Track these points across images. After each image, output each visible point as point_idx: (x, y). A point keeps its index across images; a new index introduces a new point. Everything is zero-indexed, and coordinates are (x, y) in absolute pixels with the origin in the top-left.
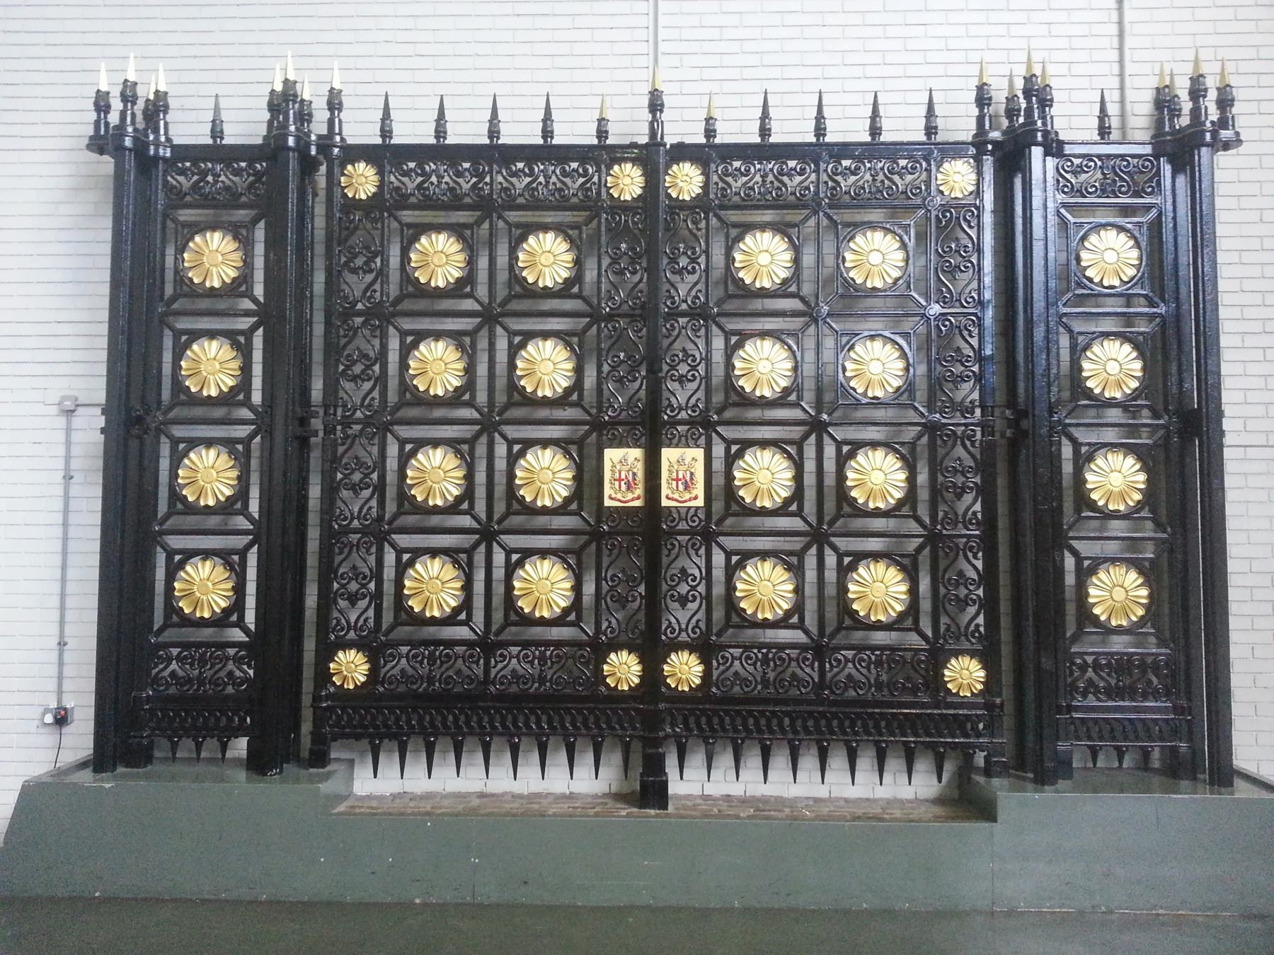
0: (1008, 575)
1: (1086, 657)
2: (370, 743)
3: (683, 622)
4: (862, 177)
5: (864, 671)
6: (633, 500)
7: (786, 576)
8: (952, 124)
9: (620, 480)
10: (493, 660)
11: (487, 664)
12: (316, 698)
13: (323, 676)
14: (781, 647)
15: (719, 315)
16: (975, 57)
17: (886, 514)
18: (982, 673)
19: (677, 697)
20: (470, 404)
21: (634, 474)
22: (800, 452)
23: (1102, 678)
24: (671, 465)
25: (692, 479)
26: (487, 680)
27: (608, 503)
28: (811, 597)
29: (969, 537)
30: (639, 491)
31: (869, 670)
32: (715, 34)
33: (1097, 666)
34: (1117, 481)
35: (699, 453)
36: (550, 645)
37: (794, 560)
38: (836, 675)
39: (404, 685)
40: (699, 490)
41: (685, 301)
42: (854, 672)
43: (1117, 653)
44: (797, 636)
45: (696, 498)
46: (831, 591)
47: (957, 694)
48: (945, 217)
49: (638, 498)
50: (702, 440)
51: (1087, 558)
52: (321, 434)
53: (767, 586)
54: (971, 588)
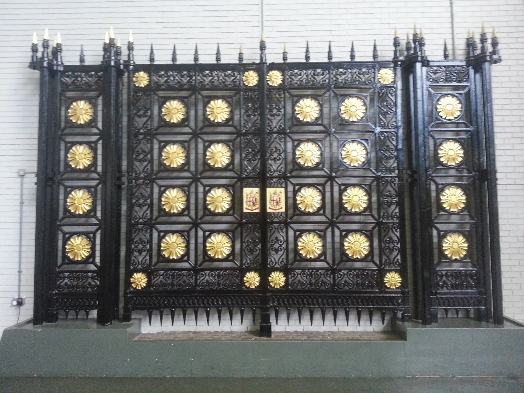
5: (352, 279)
6: (255, 209)
7: (319, 240)
8: (384, 54)
11: (334, 277)
12: (125, 293)
13: (128, 284)
14: (317, 269)
15: (290, 133)
16: (393, 26)
18: (400, 279)
19: (136, 291)
20: (188, 171)
22: (324, 189)
25: (279, 200)
26: (196, 285)
27: (245, 211)
30: (258, 206)
31: (353, 279)
33: (447, 276)
35: (282, 190)
37: (322, 233)
40: (283, 205)
42: (347, 279)
44: (324, 265)
45: (281, 208)
46: (337, 246)
49: (257, 209)
50: (284, 185)
51: (442, 231)
52: (126, 184)
54: (395, 244)
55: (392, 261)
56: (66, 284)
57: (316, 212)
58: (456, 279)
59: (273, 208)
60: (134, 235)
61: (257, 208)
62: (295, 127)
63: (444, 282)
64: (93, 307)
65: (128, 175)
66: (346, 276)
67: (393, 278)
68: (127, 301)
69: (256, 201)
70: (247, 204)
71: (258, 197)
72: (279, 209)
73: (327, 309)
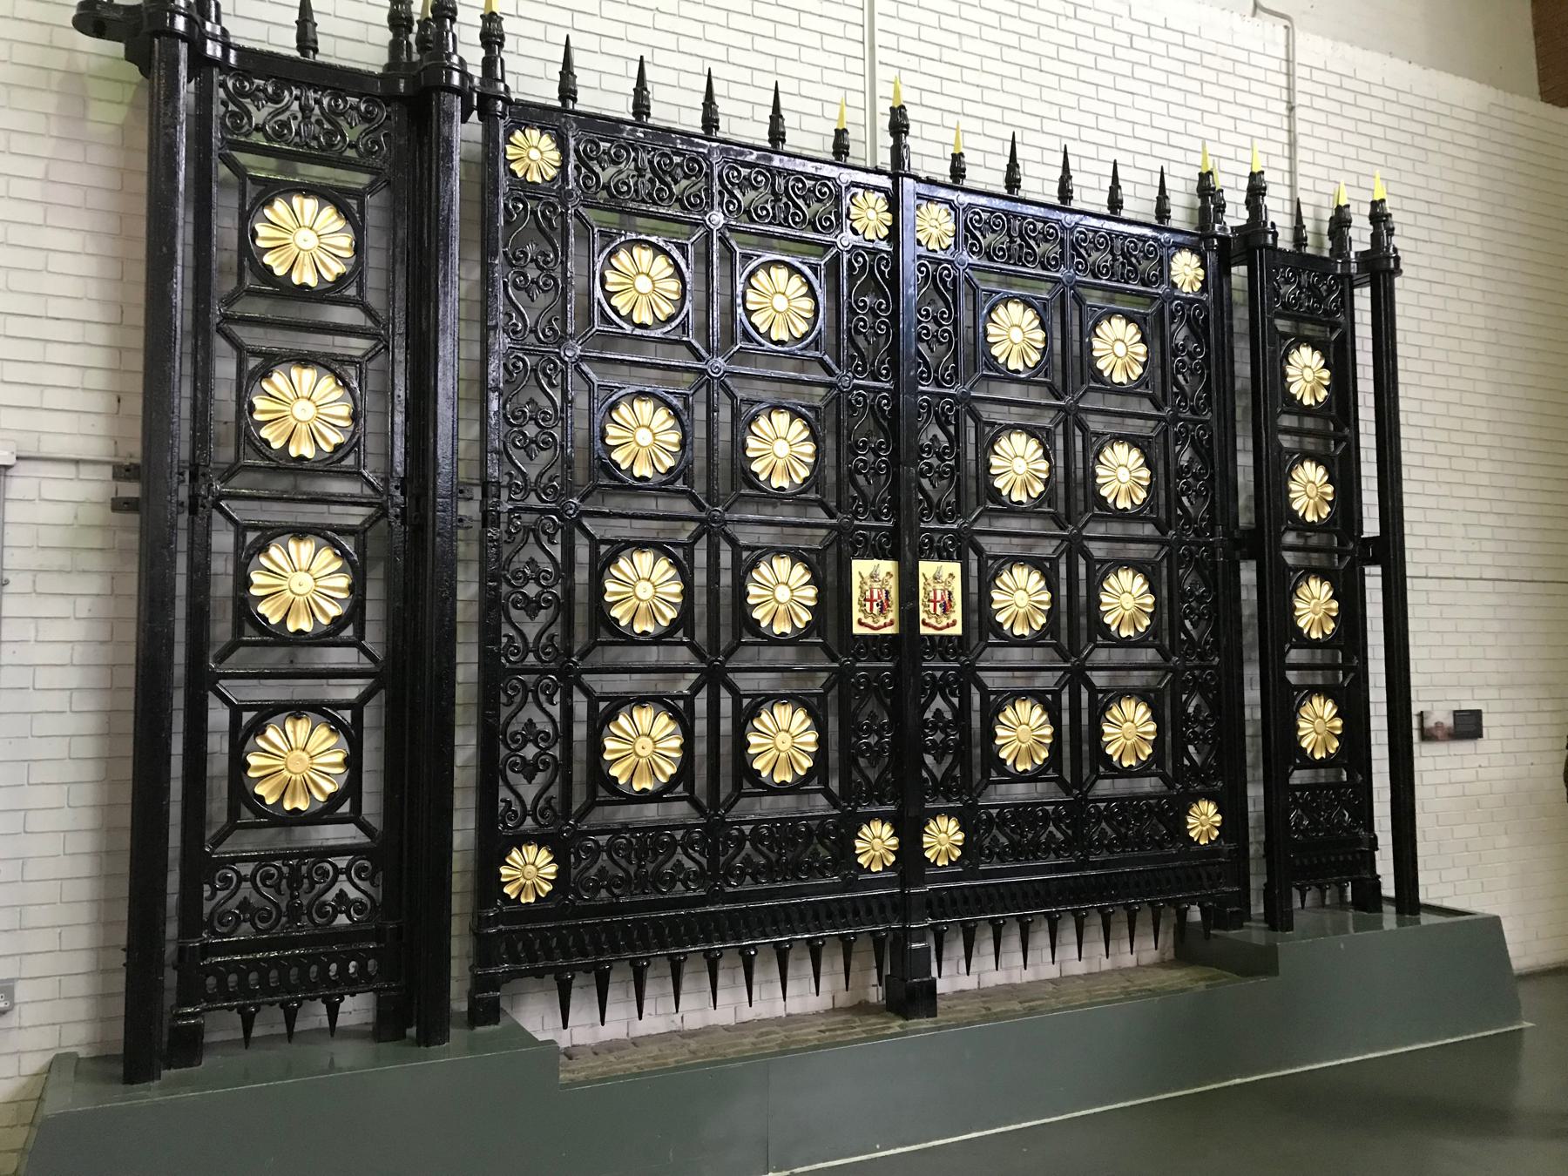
0: (381, 734)
1: (744, 827)
2: (556, 979)
3: (529, 801)
4: (287, 107)
5: (623, 863)
6: (885, 625)
9: (872, 601)
10: (206, 887)
17: (657, 640)
20: (354, 474)
21: (887, 593)
22: (690, 556)
23: (762, 853)
24: (863, 582)
27: (857, 630)
28: (581, 762)
29: (946, 669)
30: (892, 615)
31: (279, 892)
32: (934, 52)
33: (756, 838)
34: (300, 585)
35: (955, 567)
36: (308, 855)
38: (219, 905)
39: (248, 925)
40: (957, 614)
41: (534, 331)
42: (609, 865)
43: (777, 820)
44: (347, 834)
47: (868, 870)
48: (515, 208)
49: (891, 623)
51: (747, 696)
53: (301, 760)
55: (529, 807)
56: (244, 905)
57: (327, 634)
58: (640, 860)
59: (869, 621)
60: (505, 712)
61: (888, 621)
62: (249, 299)
63: (747, 860)
64: (353, 986)
65: (485, 494)
66: (343, 877)
67: (530, 867)
68: (484, 952)
69: (887, 599)
70: (861, 611)
71: (892, 585)
72: (948, 626)
73: (615, 965)
